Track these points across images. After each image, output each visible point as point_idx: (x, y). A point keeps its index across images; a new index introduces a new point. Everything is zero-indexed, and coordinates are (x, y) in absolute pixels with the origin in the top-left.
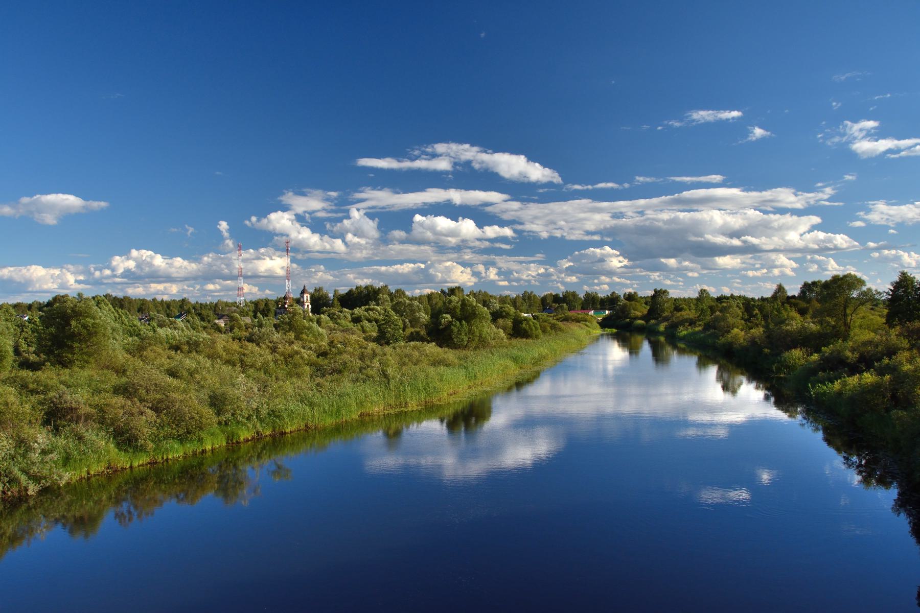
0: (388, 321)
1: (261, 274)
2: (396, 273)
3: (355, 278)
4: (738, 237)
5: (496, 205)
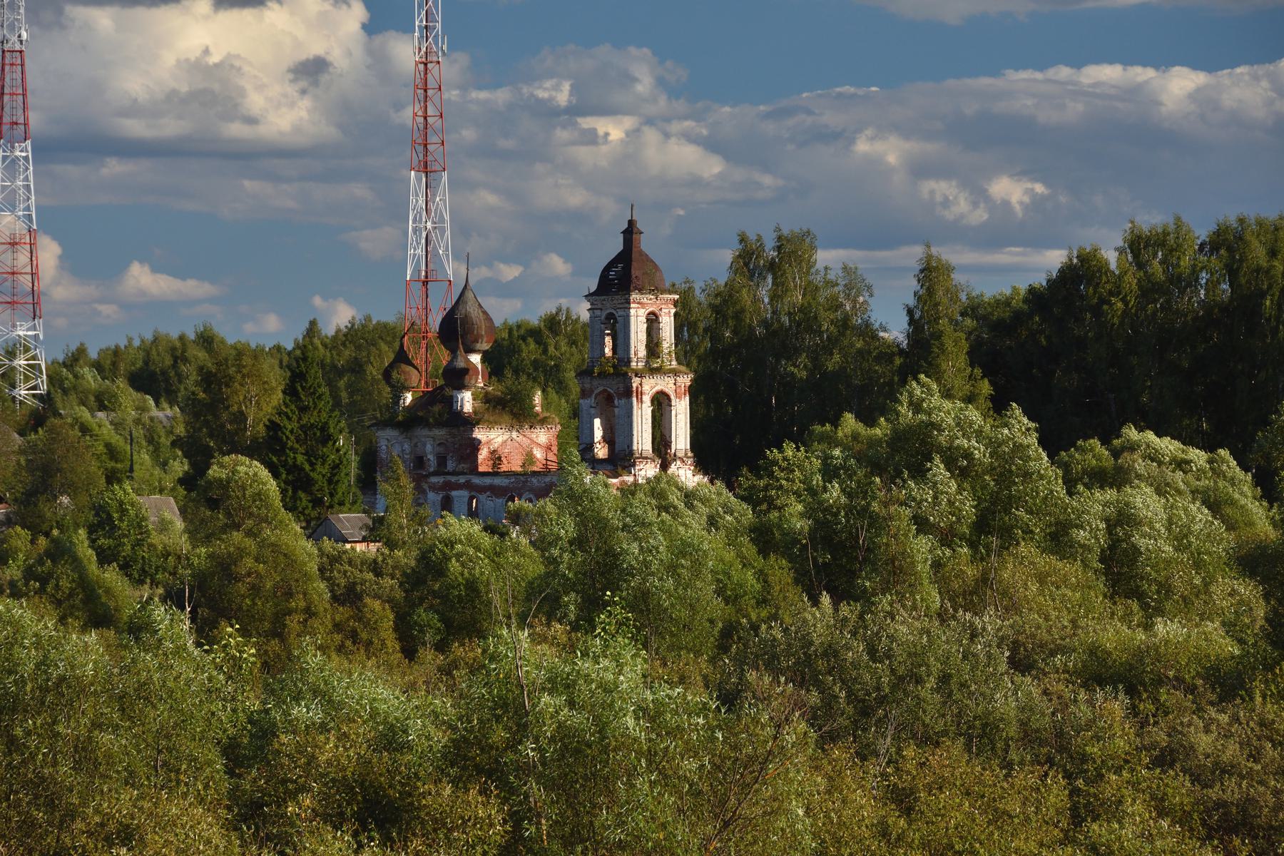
1: (136, 128)
3: (920, 170)
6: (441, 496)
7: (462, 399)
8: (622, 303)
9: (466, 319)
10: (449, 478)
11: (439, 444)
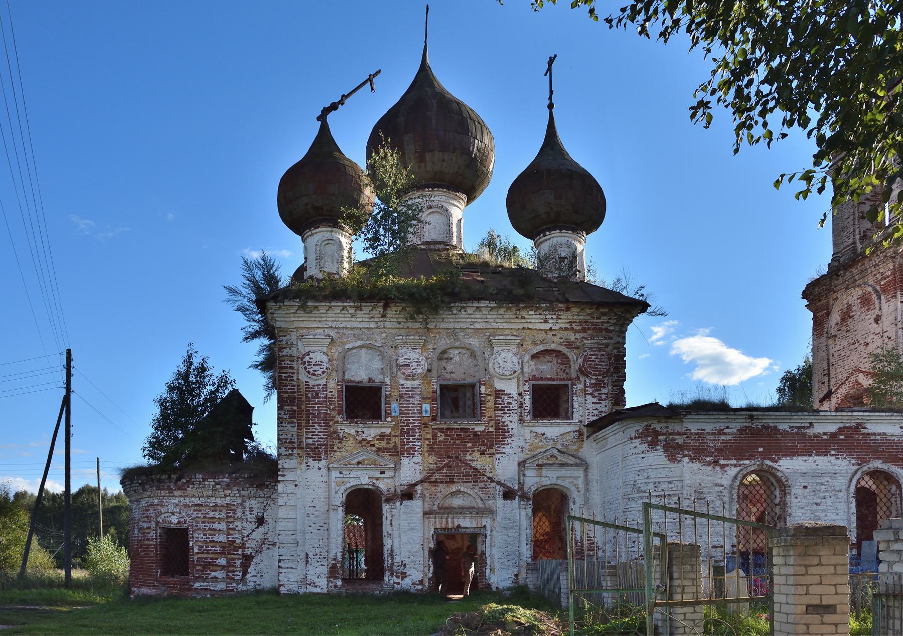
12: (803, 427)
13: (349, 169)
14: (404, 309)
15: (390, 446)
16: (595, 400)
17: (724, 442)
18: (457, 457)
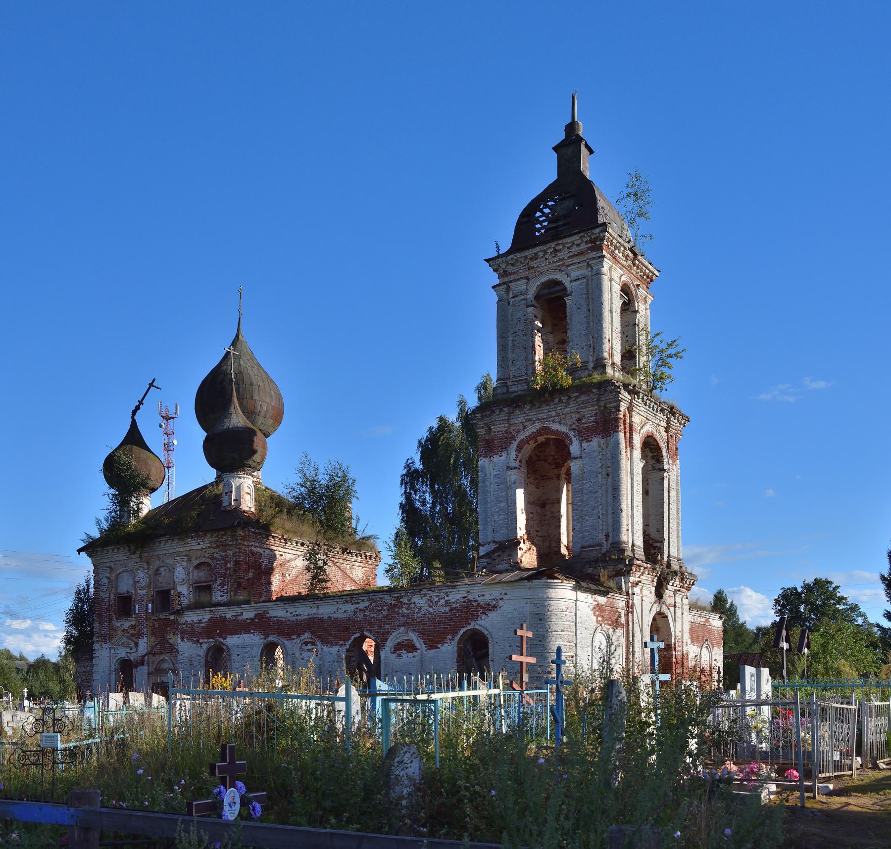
0: (563, 800)
2: (232, 396)
4: (590, 588)
5: (151, 454)
6: (205, 646)
7: (239, 488)
8: (581, 253)
9: (227, 374)
10: (221, 611)
11: (197, 567)
12: (238, 615)
13: (235, 429)
14: (450, 744)
15: (136, 632)
16: (221, 594)
17: (203, 628)
18: (164, 637)
